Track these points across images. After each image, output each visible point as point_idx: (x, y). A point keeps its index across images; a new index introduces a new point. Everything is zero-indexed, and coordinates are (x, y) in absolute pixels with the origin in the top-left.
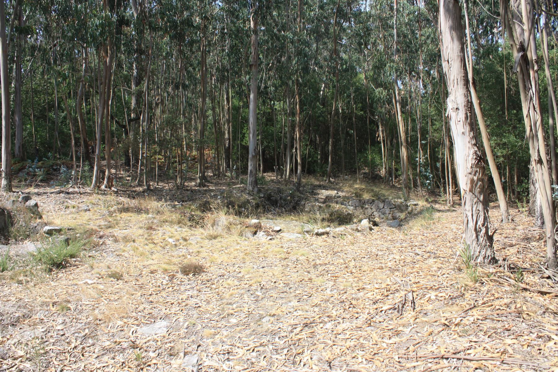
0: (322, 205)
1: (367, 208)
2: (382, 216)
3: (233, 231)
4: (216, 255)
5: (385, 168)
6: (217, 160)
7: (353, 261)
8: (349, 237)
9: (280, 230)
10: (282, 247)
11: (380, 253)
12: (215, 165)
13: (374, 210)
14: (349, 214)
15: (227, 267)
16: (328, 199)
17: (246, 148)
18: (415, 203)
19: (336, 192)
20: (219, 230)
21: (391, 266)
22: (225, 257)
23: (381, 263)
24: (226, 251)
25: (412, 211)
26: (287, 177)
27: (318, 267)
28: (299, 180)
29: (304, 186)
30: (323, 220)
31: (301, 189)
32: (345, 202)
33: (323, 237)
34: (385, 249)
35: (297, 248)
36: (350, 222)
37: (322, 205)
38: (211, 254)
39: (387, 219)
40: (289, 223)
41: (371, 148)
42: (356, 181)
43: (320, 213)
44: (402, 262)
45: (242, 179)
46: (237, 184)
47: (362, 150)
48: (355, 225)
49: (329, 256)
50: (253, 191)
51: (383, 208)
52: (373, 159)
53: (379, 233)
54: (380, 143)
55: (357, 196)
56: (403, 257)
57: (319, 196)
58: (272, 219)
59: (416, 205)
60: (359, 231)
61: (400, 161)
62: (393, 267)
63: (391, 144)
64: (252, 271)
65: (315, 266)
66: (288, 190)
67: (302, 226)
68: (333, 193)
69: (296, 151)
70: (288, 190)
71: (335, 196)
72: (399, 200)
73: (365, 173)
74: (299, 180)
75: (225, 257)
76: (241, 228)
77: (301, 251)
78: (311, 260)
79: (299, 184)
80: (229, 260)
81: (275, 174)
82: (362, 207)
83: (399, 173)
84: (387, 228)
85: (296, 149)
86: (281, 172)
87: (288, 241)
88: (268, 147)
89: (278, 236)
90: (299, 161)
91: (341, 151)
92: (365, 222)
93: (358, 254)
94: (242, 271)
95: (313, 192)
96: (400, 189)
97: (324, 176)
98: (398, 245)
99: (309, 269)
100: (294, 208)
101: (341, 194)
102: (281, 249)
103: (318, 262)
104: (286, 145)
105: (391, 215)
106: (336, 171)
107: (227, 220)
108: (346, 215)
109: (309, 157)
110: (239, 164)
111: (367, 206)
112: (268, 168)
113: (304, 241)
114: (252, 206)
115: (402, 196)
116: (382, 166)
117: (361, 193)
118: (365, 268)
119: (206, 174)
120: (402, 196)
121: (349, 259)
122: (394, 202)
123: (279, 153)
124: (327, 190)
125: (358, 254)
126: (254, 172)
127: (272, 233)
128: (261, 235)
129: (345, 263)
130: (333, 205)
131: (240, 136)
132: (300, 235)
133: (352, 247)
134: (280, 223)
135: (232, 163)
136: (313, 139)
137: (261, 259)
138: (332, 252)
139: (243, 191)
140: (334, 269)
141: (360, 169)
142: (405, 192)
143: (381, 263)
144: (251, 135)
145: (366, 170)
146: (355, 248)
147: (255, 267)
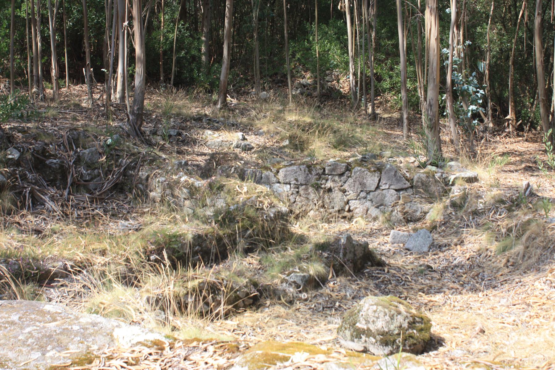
1: (330, 190)
2: (374, 212)
5: (355, 74)
18: (469, 174)
19: (240, 135)
25: (464, 197)
42: (284, 104)
47: (300, 33)
51: (378, 187)
52: (325, 53)
59: (471, 180)
82: (317, 187)
95: (179, 134)
97: (211, 92)
100: (119, 188)
101: (253, 140)
109: (179, 49)
117: (305, 136)
124: (217, 129)
130: (233, 183)
145: (308, 79)
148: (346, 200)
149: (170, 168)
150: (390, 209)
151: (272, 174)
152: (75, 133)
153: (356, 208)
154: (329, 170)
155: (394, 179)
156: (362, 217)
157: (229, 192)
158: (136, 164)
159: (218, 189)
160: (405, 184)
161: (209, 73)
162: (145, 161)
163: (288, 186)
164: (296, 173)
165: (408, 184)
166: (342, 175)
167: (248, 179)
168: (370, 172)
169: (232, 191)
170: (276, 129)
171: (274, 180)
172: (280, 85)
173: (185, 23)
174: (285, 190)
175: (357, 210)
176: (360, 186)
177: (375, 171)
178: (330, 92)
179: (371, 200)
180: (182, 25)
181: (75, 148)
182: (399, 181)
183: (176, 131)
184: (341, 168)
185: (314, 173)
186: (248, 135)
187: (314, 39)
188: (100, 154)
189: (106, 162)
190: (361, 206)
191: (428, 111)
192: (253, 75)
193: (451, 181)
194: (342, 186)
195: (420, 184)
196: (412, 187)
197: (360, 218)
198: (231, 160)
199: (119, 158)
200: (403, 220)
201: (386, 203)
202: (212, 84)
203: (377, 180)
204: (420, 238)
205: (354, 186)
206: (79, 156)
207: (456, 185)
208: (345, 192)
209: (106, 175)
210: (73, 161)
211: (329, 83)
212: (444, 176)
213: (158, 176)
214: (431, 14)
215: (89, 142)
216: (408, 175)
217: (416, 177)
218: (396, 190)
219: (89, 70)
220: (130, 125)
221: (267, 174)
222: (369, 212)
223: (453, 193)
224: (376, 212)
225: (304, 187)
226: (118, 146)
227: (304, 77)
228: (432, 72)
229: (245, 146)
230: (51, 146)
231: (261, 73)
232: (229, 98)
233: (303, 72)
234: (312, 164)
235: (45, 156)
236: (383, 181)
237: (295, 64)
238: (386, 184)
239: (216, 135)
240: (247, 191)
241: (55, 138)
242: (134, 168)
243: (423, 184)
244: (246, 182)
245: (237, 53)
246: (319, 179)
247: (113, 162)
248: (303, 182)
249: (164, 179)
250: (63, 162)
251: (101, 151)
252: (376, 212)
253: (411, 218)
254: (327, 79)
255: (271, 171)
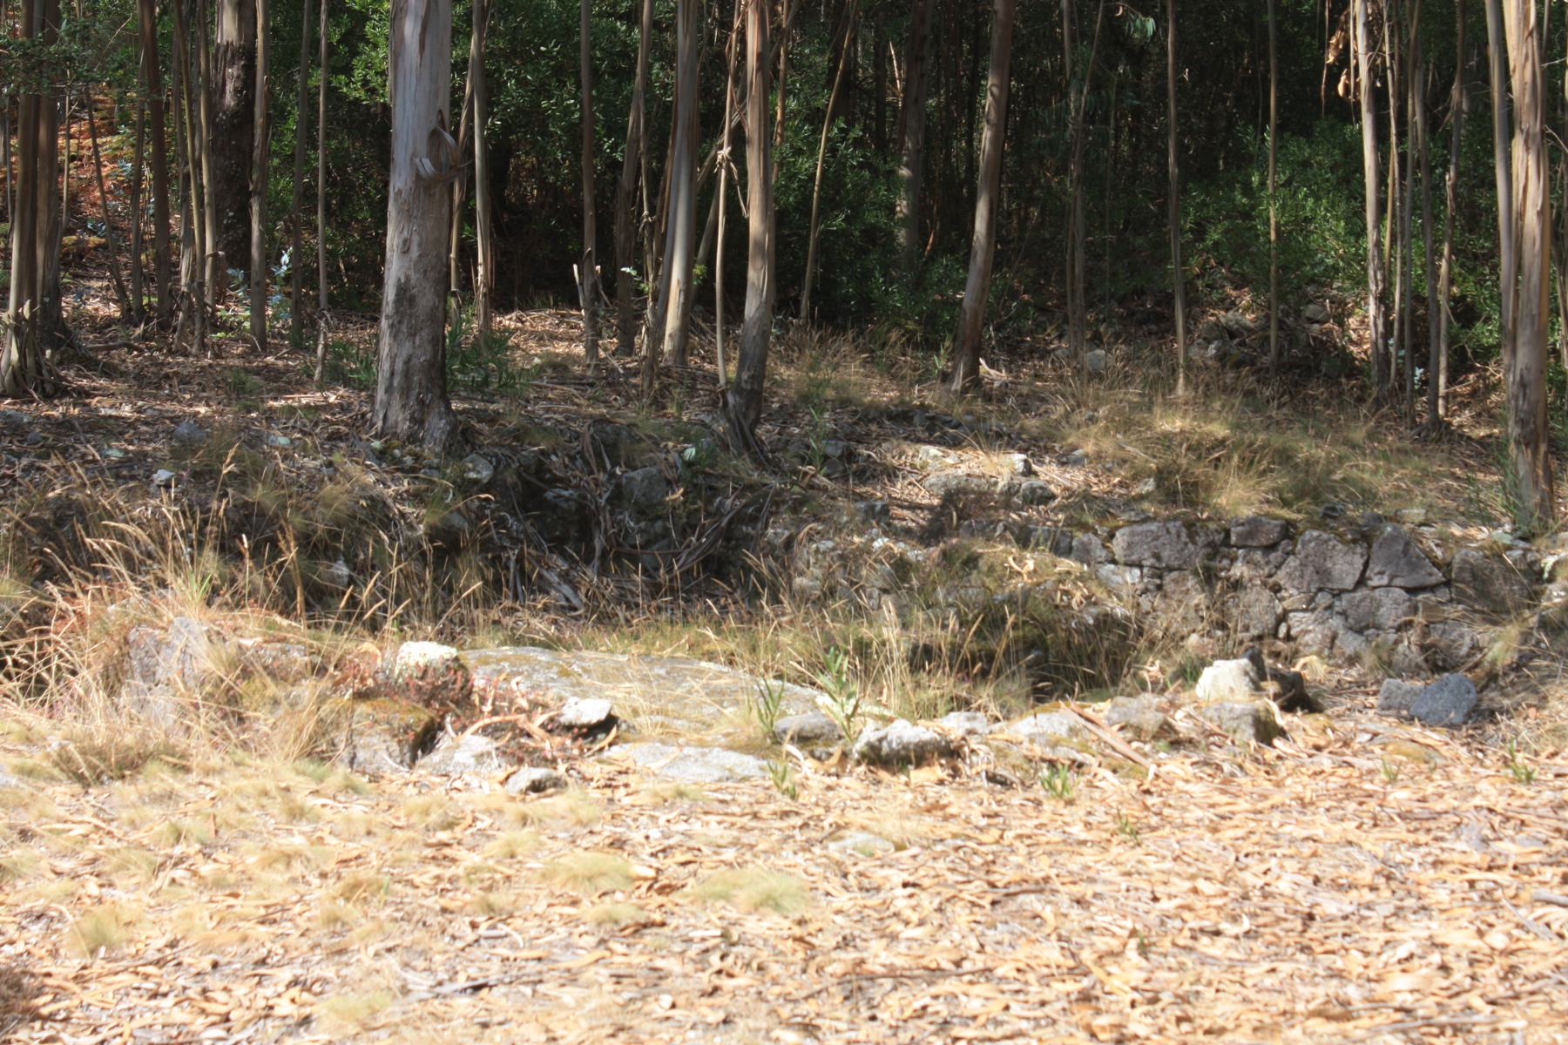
0: (915, 554)
2: (1350, 643)
3: (262, 720)
4: (127, 896)
5: (1384, 299)
6: (150, 201)
7: (1132, 953)
8: (1109, 781)
9: (609, 723)
10: (618, 844)
11: (1330, 904)
12: (141, 244)
13: (1292, 596)
14: (1107, 622)
15: (214, 982)
16: (961, 509)
17: (374, 127)
19: (1017, 459)
20: (158, 712)
21: (1408, 1000)
22: (195, 913)
23: (1338, 974)
24: (207, 869)
26: (667, 346)
27: (876, 993)
28: (756, 366)
29: (788, 415)
30: (921, 658)
31: (766, 432)
32: (1080, 537)
33: (919, 776)
34: (1365, 876)
35: (729, 854)
36: (1115, 679)
37: (915, 554)
38: (92, 887)
39: (1388, 666)
40: (674, 676)
41: (1280, 147)
43: (902, 612)
44: (1489, 974)
45: (339, 351)
46: (300, 385)
47: (1218, 160)
48: (1148, 698)
49: (961, 915)
50: (412, 438)
51: (1361, 582)
53: (1325, 761)
54: (1347, 111)
55: (1168, 495)
56: (1497, 939)
57: (899, 489)
58: (549, 645)
60: (1176, 744)
61: (1494, 252)
62: (1426, 1007)
63: (1433, 122)
64: (392, 1011)
65: (856, 985)
66: (677, 436)
67: (769, 697)
68: (1001, 467)
69: (738, 156)
70: (677, 436)
71: (1010, 491)
72: (1482, 534)
73: (1230, 333)
74: (756, 366)
75: (195, 913)
76: (322, 699)
77: (759, 876)
78: (825, 941)
79: (753, 394)
80: (225, 935)
81: (579, 318)
82: (1209, 578)
83: (1486, 333)
84: (1386, 725)
85: (739, 140)
86: (622, 306)
87: (663, 802)
88: (529, 119)
89: (591, 767)
90: (756, 223)
91: (1062, 169)
92: (1225, 683)
93: (1166, 905)
94: (319, 1009)
95: (850, 456)
96: (1489, 453)
97: (932, 346)
98: (1462, 848)
99: (809, 1008)
101: (1051, 474)
102: (615, 860)
103: (878, 955)
104: (668, 109)
105: (1413, 636)
106: (1022, 314)
107: (216, 637)
108: (1088, 631)
109: (830, 204)
110: (317, 243)
111: (1239, 570)
112: (530, 277)
113: (784, 803)
114: (412, 550)
115: (1497, 503)
116: (1361, 281)
117: (1199, 470)
118: (1222, 1009)
119: (68, 302)
120: (1497, 503)
121: (1103, 943)
122: (1443, 540)
123: (615, 166)
124: (955, 444)
125: (1166, 905)
126: (426, 300)
127: (549, 745)
128: (463, 756)
129: (1077, 971)
130: (1001, 552)
131: (327, 32)
132: (749, 764)
133: (1130, 857)
134: (619, 674)
135: (267, 231)
136: (866, 73)
137: (461, 926)
138: (978, 885)
139: (342, 434)
140: (995, 1009)
141: (1194, 304)
142: (1523, 470)
143: (1338, 974)
144: (411, 29)
145: (1245, 311)
146: (1152, 864)
147: (420, 983)
148: (1279, 610)
149: (845, 519)
150: (1393, 637)
151: (1096, 541)
152: (608, 429)
153: (1307, 632)
154: (1239, 535)
155: (1402, 562)
156: (1319, 654)
157: (991, 569)
158: (759, 510)
159: (966, 563)
160: (1430, 574)
161: (919, 285)
162: (784, 502)
163: (1137, 572)
164: (1157, 538)
165: (1438, 576)
166: (1270, 548)
167: (1037, 544)
168: (1345, 543)
169: (999, 568)
170: (1122, 448)
171: (1101, 554)
172: (1154, 327)
173: (850, 124)
174: (1129, 580)
175: (1307, 638)
176: (1316, 577)
177: (1354, 541)
178: (1316, 355)
179: (1344, 614)
180: (841, 130)
181: (609, 466)
182: (1414, 566)
183: (841, 444)
184: (1271, 531)
185: (1201, 540)
186: (1042, 463)
187: (1263, 184)
188: (669, 483)
189: (684, 503)
190: (1319, 628)
191: (1517, 399)
192: (1065, 297)
193: (1547, 569)
194: (1270, 576)
195: (1467, 576)
196: (1448, 583)
197: (1315, 658)
198: (996, 509)
199: (715, 496)
200: (1424, 666)
201: (1382, 620)
202: (931, 322)
203: (1359, 562)
204: (1446, 694)
205: (1302, 576)
206: (619, 486)
207: (1559, 579)
208: (1279, 590)
209: (684, 534)
210: (605, 496)
211: (1316, 326)
212: (1530, 557)
213: (817, 537)
214: (1527, 149)
215: (643, 452)
216: (1439, 553)
217: (1457, 558)
218: (1409, 590)
219: (593, 271)
220: (729, 420)
221: (1085, 539)
222: (1337, 642)
223: (1549, 599)
224: (1356, 643)
225: (1175, 574)
226: (712, 467)
227: (1233, 305)
228: (1529, 300)
229: (1033, 490)
230: (554, 458)
231: (1089, 288)
232: (984, 366)
233: (1229, 290)
234: (1199, 519)
235: (542, 480)
236: (1375, 568)
237: (1206, 261)
238: (1381, 573)
239: (949, 461)
240: (1035, 571)
241: (561, 439)
242: (753, 520)
243: (1475, 576)
244: (1033, 551)
245: (1010, 214)
246: (1211, 557)
247: (700, 504)
248: (1176, 564)
249: (830, 544)
250: (585, 498)
251: (671, 475)
252: (1356, 643)
253: (1444, 661)
254: (1308, 314)
255: (1095, 533)
